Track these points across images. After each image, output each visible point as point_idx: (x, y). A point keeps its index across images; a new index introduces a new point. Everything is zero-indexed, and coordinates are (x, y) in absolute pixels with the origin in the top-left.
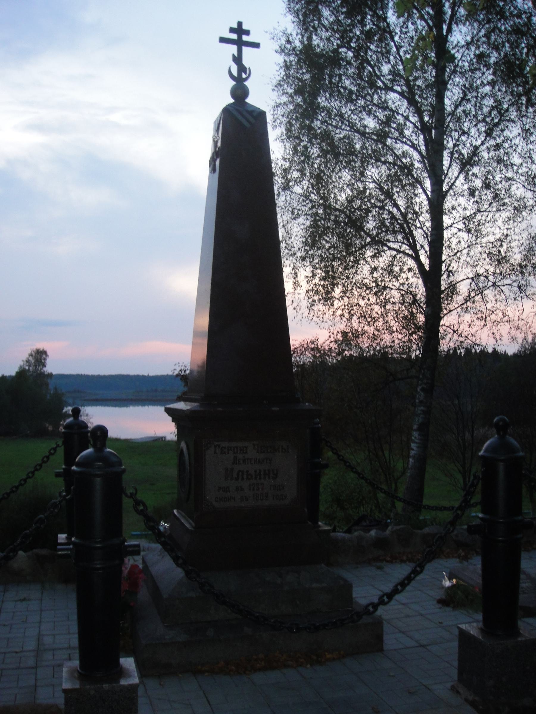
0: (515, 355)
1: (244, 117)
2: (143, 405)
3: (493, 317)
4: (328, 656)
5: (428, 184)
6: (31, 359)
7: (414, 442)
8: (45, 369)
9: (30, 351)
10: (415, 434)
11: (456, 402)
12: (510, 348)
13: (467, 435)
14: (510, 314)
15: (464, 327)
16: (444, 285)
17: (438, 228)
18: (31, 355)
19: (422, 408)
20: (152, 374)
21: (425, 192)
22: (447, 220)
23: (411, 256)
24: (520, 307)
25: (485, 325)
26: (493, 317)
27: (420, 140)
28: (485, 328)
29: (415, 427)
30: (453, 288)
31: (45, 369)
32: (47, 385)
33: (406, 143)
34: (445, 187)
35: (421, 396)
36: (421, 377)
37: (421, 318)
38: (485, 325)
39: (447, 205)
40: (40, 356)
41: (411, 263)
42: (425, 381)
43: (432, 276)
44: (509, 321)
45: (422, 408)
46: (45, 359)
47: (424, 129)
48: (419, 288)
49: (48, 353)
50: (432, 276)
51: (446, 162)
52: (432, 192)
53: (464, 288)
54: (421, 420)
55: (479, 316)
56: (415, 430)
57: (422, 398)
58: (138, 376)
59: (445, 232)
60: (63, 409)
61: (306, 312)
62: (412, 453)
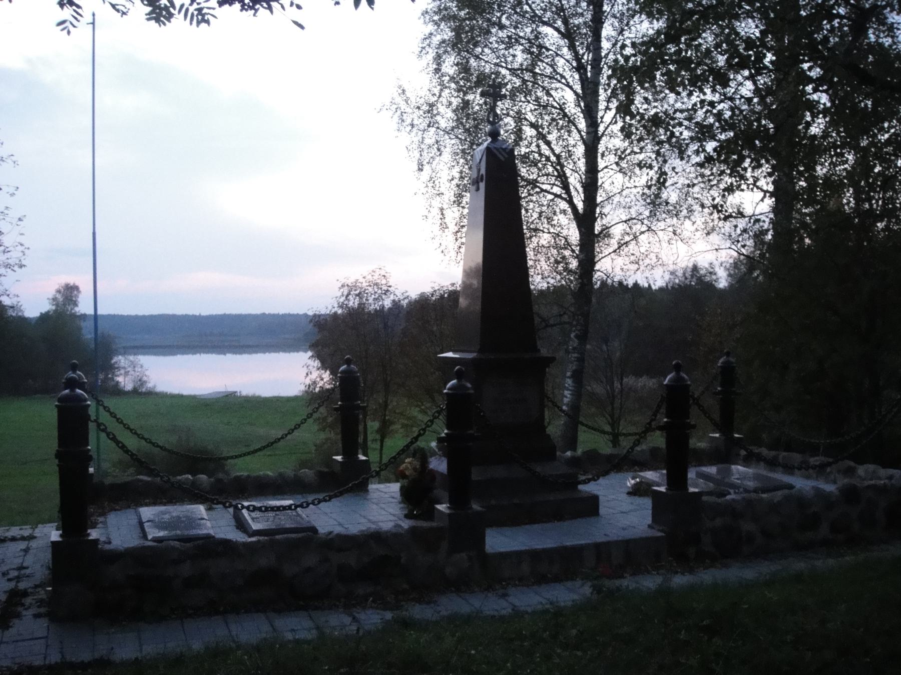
0: (661, 289)
1: (500, 153)
2: (264, 352)
3: (647, 261)
4: (583, 478)
5: (582, 124)
6: (59, 296)
7: (568, 390)
8: (77, 309)
9: (57, 287)
10: (569, 382)
11: (605, 348)
12: (658, 279)
13: (617, 385)
14: (664, 258)
15: (610, 266)
16: (597, 229)
17: (592, 170)
18: (59, 291)
19: (576, 355)
20: (205, 313)
21: (579, 132)
22: (601, 164)
23: (565, 199)
24: (674, 251)
25: (638, 269)
26: (647, 261)
27: (574, 79)
28: (638, 272)
29: (569, 374)
30: (606, 233)
31: (77, 309)
32: (80, 329)
33: (560, 82)
34: (601, 128)
35: (574, 343)
36: (574, 323)
37: (574, 264)
38: (638, 269)
39: (601, 148)
40: (69, 293)
41: (564, 205)
42: (579, 327)
43: (586, 220)
44: (663, 265)
45: (576, 355)
46: (77, 296)
47: (580, 68)
48: (573, 234)
49: (81, 289)
50: (586, 220)
51: (602, 105)
52: (588, 133)
53: (617, 231)
54: (574, 368)
55: (632, 258)
56: (569, 377)
57: (575, 345)
58: (109, 315)
59: (600, 175)
60: (112, 359)
61: (453, 254)
62: (566, 400)
